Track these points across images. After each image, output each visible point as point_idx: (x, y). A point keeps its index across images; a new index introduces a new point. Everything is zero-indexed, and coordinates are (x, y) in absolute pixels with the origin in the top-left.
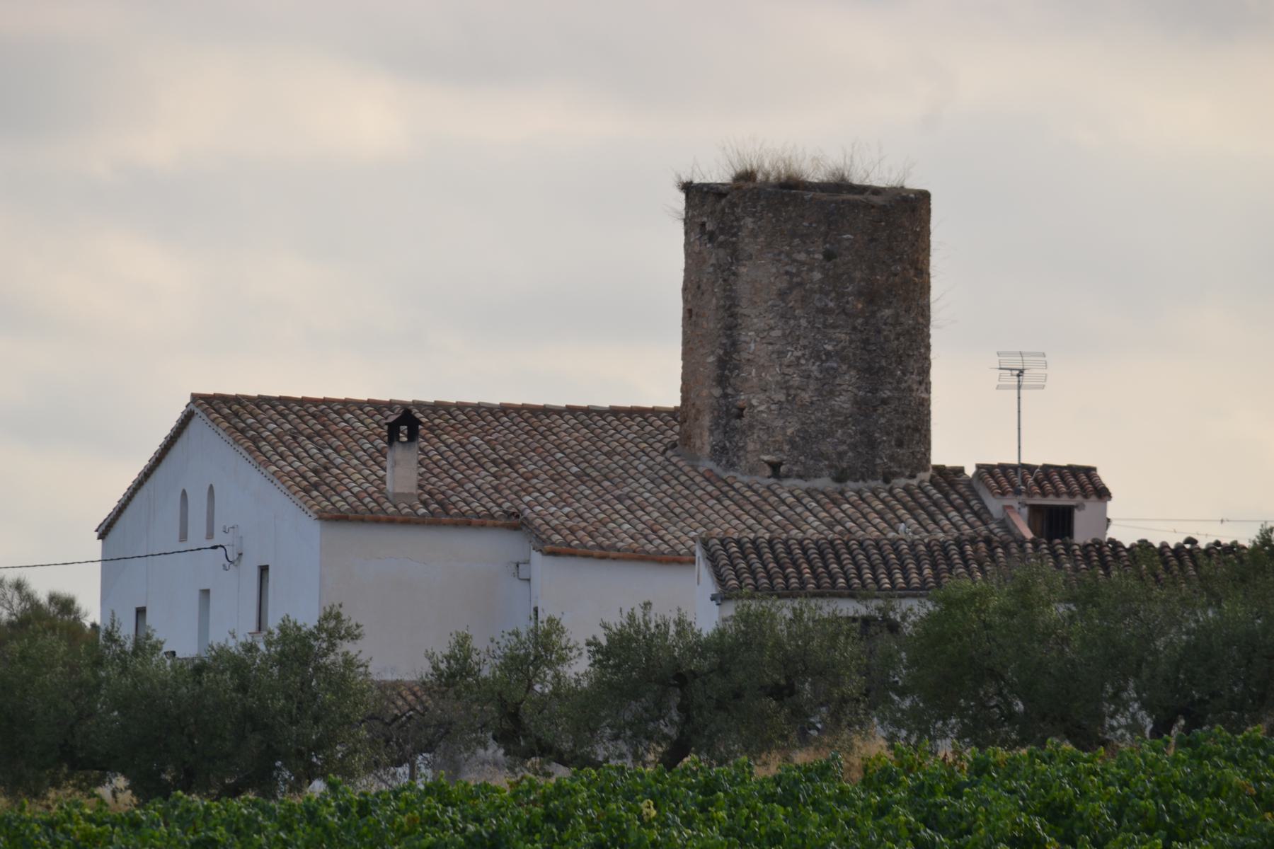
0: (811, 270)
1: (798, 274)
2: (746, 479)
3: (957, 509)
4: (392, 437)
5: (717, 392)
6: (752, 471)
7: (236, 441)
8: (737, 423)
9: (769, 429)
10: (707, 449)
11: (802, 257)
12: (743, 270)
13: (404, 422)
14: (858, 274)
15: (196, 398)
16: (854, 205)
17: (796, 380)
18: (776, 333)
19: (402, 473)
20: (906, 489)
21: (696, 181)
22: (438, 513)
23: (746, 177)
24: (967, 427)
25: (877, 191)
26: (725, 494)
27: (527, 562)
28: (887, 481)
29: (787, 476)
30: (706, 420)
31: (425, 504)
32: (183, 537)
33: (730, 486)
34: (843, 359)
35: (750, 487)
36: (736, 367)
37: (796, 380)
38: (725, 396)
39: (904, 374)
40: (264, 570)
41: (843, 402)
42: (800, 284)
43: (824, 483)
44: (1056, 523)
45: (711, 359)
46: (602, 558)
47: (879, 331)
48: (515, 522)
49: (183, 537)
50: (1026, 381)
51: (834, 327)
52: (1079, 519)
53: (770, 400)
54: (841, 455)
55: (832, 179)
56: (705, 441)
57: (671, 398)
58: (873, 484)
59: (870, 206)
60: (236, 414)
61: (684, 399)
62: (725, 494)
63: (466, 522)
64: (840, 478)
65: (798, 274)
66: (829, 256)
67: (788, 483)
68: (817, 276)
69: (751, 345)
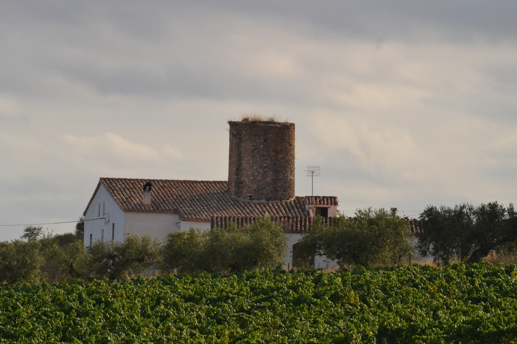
0: (260, 144)
1: (257, 146)
2: (243, 200)
3: (297, 208)
4: (145, 189)
5: (236, 177)
6: (245, 198)
7: (108, 190)
8: (241, 185)
9: (249, 187)
10: (234, 192)
11: (258, 141)
12: (243, 145)
13: (148, 185)
14: (273, 146)
15: (101, 179)
16: (272, 127)
17: (256, 174)
18: (251, 161)
19: (147, 199)
20: (286, 203)
21: (233, 121)
22: (156, 208)
23: (246, 120)
24: (302, 188)
25: (279, 123)
26: (236, 204)
27: (180, 223)
28: (281, 201)
29: (254, 200)
30: (233, 185)
31: (153, 207)
32: (99, 216)
33: (238, 202)
34: (269, 168)
35: (243, 202)
36: (241, 170)
37: (256, 174)
38: (238, 178)
39: (286, 172)
40: (114, 224)
41: (269, 180)
42: (257, 148)
43: (264, 201)
44: (323, 212)
45: (235, 168)
46: (197, 221)
47: (279, 161)
48: (176, 212)
49: (99, 216)
50: (314, 174)
51: (266, 160)
52: (329, 211)
53: (249, 179)
54: (268, 194)
55: (270, 120)
56: (233, 190)
57: (227, 180)
58: (277, 201)
59: (276, 127)
60: (111, 183)
61: (229, 179)
62: (236, 204)
63: (163, 211)
64: (268, 200)
65: (257, 146)
66: (265, 141)
67: (254, 201)
68: (262, 146)
69: (245, 165)
